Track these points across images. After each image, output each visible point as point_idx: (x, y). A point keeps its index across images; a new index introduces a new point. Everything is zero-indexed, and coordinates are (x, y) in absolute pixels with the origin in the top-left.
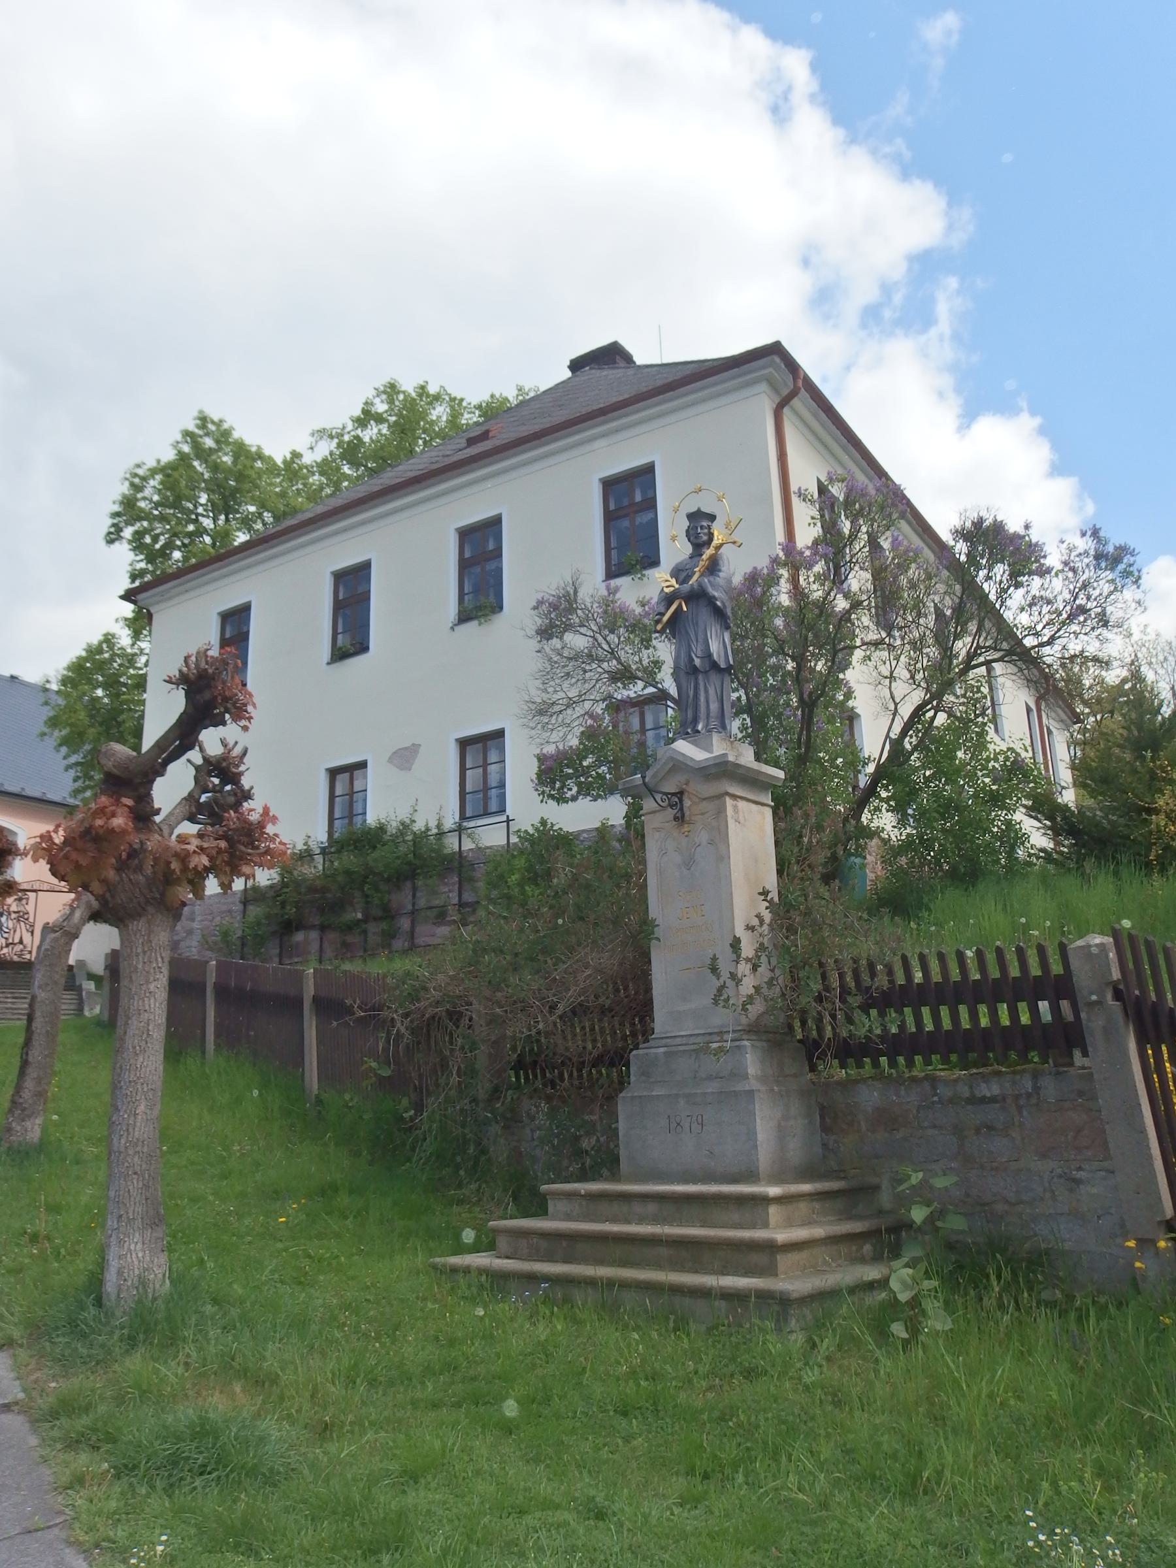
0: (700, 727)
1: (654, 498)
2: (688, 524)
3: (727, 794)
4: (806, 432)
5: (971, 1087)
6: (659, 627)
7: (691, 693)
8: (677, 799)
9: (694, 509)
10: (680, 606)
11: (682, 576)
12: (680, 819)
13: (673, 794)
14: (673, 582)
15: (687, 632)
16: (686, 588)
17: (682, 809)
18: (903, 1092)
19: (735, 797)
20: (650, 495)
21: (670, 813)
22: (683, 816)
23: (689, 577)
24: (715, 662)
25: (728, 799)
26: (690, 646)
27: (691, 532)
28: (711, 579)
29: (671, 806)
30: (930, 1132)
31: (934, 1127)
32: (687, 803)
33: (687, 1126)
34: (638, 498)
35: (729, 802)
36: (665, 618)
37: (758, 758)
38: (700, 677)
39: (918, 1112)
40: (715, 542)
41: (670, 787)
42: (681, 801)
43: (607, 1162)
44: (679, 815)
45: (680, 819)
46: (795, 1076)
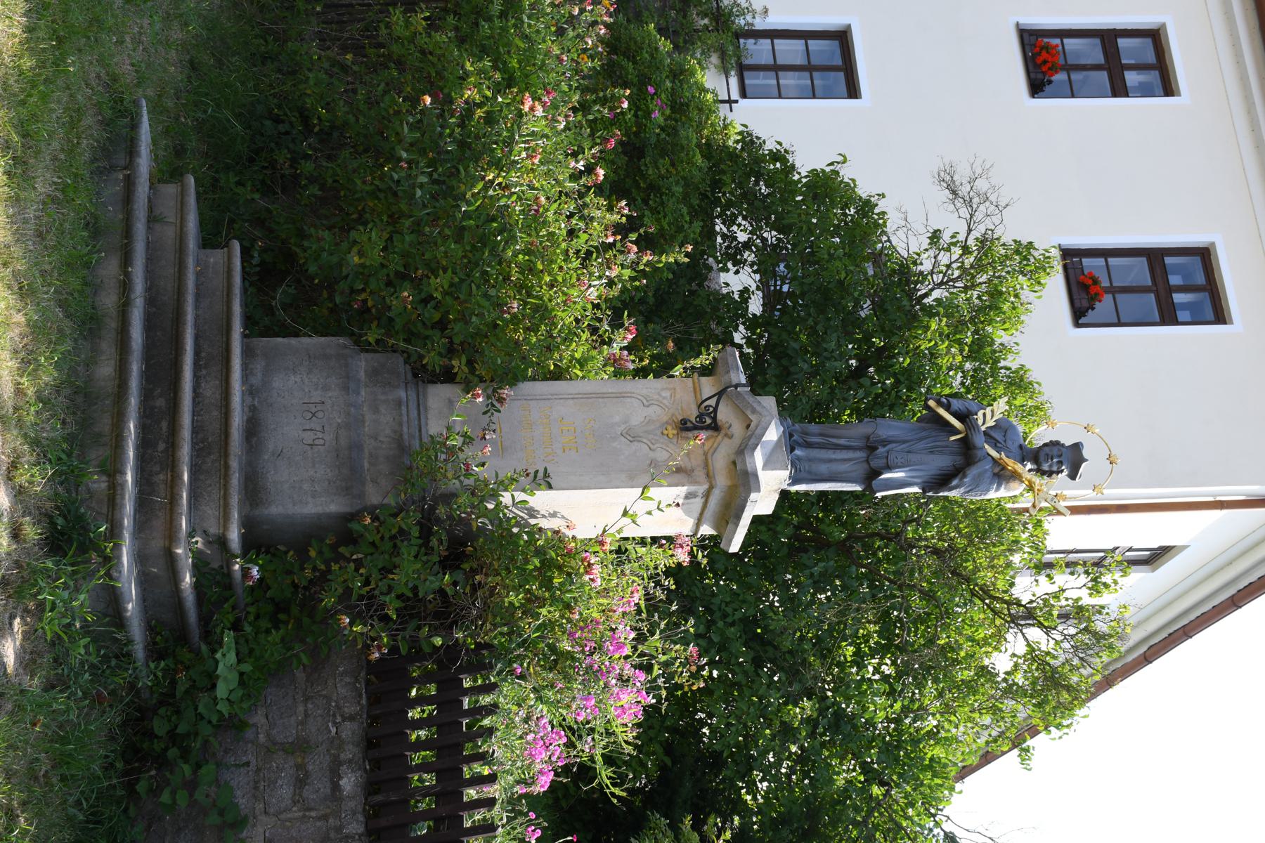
0: (798, 452)
1: (1175, 322)
2: (1067, 444)
3: (711, 487)
4: (1158, 604)
5: (350, 761)
6: (932, 403)
7: (842, 442)
8: (706, 422)
9: (1085, 453)
10: (957, 432)
11: (998, 436)
12: (685, 427)
13: (714, 419)
14: (990, 423)
15: (921, 439)
16: (979, 440)
17: (695, 428)
18: (348, 679)
19: (707, 495)
20: (1182, 315)
21: (692, 414)
22: (688, 429)
23: (995, 444)
24: (881, 474)
25: (706, 486)
26: (904, 442)
27: (1055, 451)
28: (989, 474)
29: (700, 416)
30: (301, 709)
31: (306, 715)
32: (703, 435)
33: (314, 424)
34: (1178, 298)
35: (701, 489)
36: (942, 412)
37: (757, 520)
38: (860, 455)
39: (325, 697)
40: (1037, 480)
41: (725, 414)
42: (708, 428)
43: (261, 324)
44: (689, 425)
45: (685, 427)
46: (560, 568)
